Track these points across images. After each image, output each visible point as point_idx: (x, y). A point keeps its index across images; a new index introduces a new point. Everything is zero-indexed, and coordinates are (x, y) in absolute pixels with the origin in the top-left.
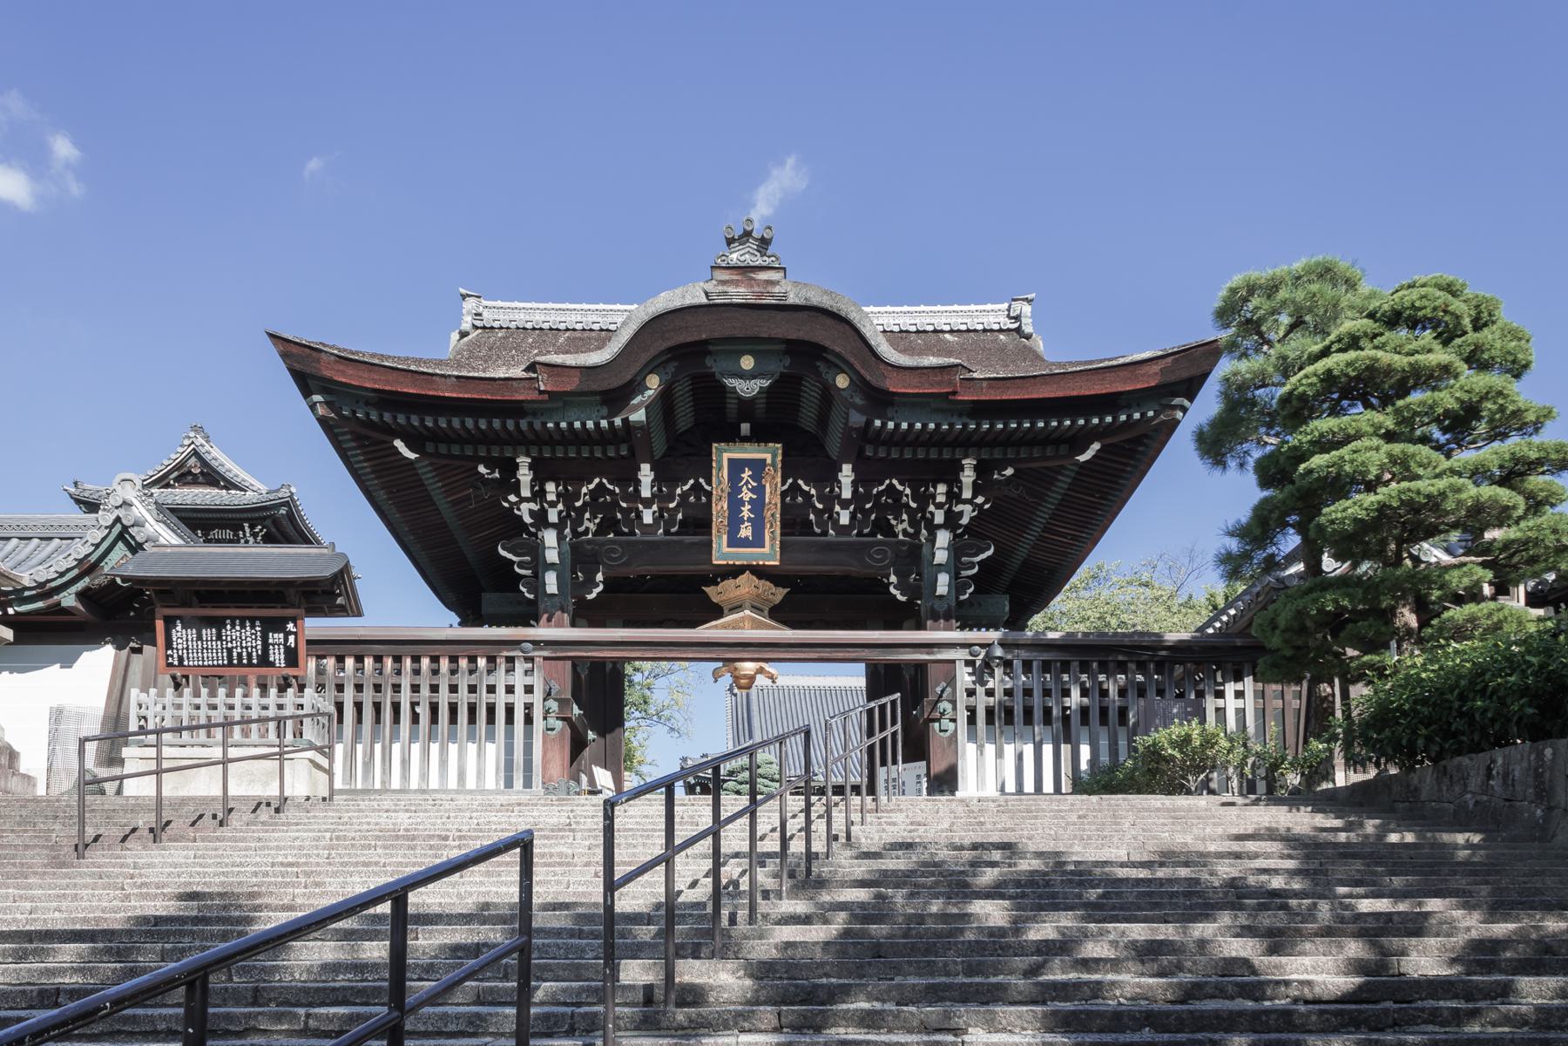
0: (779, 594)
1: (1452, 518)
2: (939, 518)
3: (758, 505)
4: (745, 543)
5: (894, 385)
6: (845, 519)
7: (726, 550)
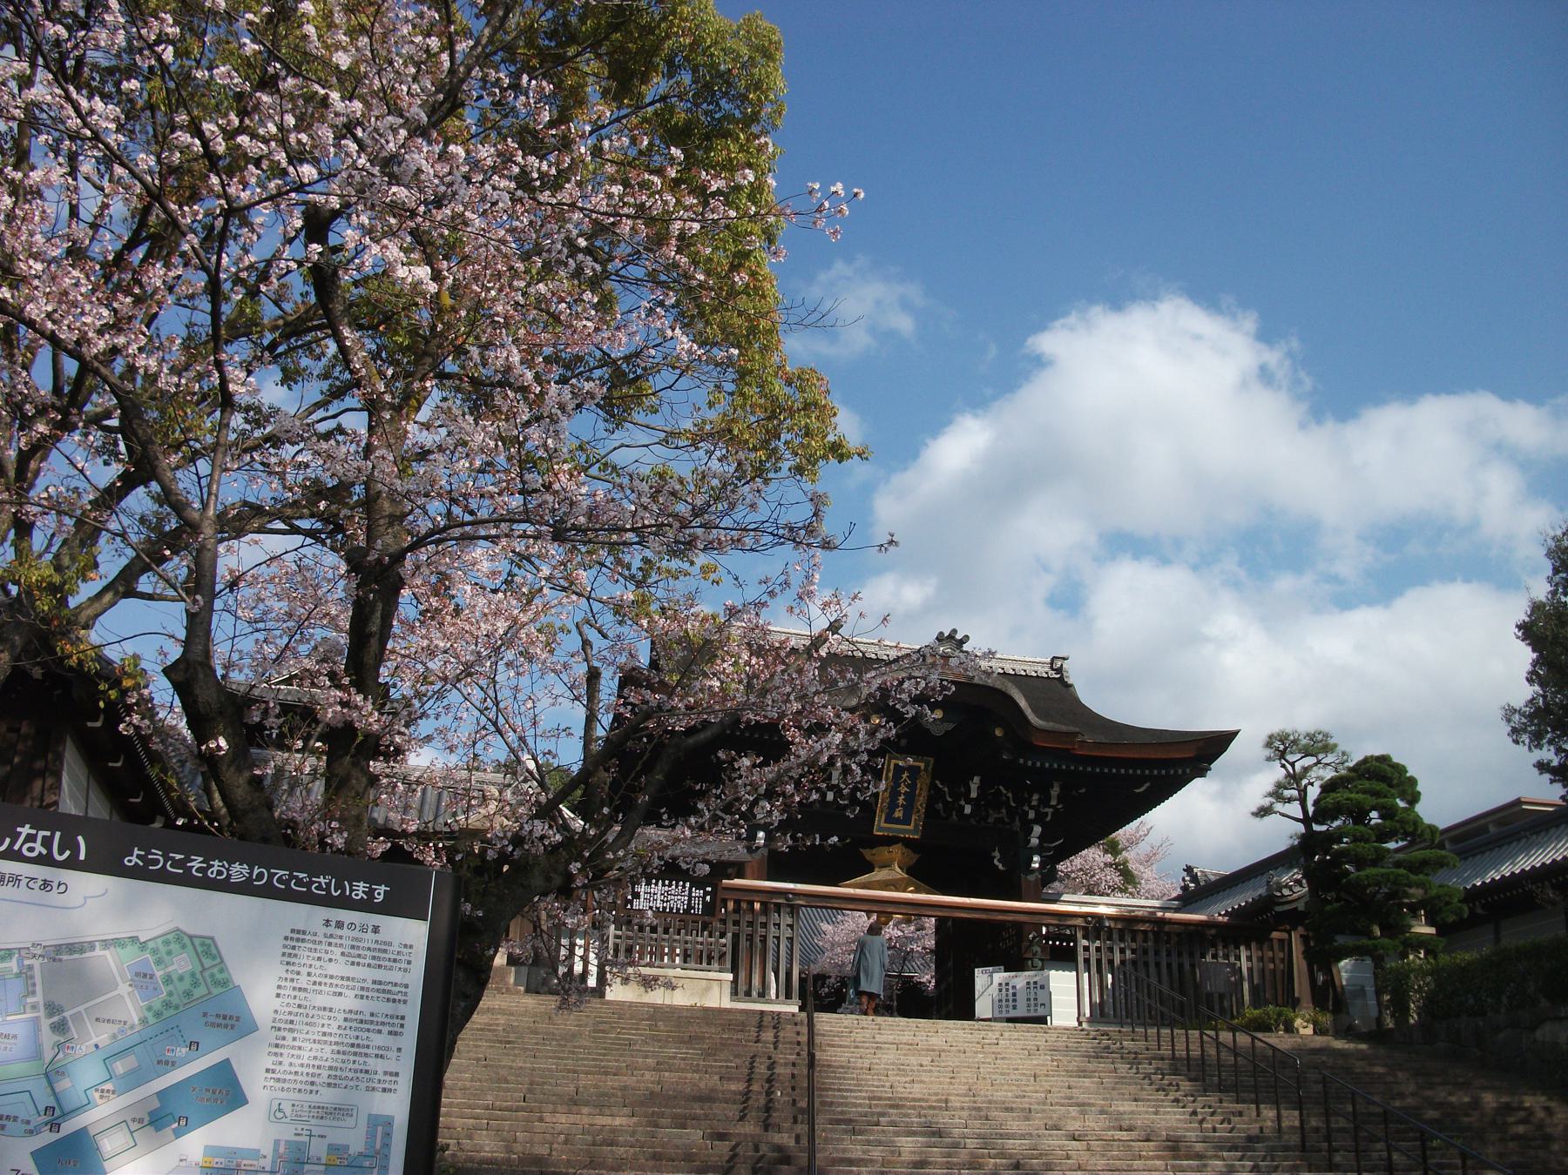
1: (115, 305)
2: (1032, 815)
3: (910, 797)
4: (897, 821)
5: (1039, 742)
6: (968, 810)
7: (883, 825)
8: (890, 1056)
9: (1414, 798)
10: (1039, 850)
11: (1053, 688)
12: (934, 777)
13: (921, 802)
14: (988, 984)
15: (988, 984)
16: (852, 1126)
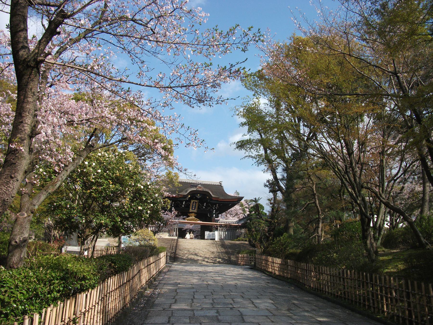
0: (196, 215)
3: (195, 206)
8: (187, 244)
9: (263, 209)
10: (215, 214)
11: (219, 188)
12: (199, 203)
13: (197, 207)
14: (207, 233)
15: (207, 233)
16: (180, 250)
